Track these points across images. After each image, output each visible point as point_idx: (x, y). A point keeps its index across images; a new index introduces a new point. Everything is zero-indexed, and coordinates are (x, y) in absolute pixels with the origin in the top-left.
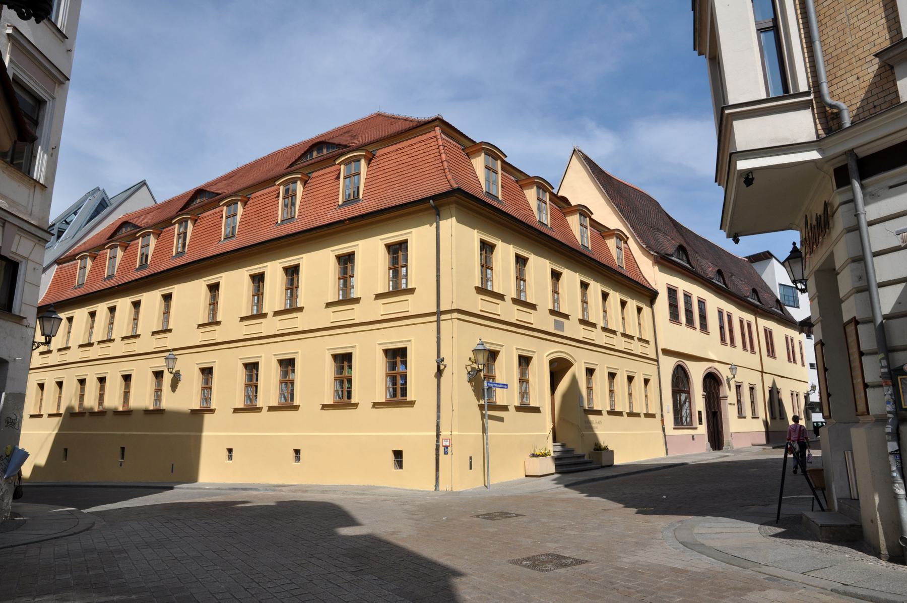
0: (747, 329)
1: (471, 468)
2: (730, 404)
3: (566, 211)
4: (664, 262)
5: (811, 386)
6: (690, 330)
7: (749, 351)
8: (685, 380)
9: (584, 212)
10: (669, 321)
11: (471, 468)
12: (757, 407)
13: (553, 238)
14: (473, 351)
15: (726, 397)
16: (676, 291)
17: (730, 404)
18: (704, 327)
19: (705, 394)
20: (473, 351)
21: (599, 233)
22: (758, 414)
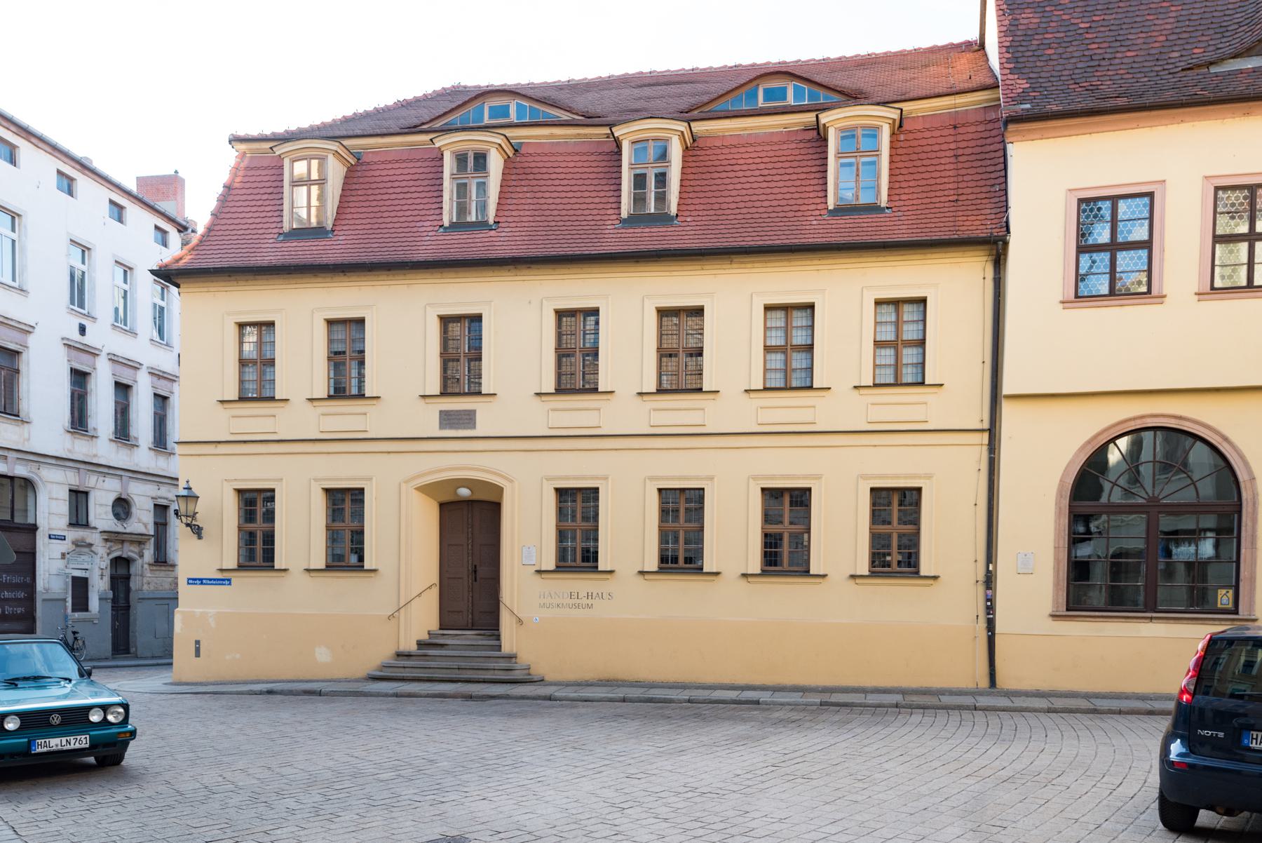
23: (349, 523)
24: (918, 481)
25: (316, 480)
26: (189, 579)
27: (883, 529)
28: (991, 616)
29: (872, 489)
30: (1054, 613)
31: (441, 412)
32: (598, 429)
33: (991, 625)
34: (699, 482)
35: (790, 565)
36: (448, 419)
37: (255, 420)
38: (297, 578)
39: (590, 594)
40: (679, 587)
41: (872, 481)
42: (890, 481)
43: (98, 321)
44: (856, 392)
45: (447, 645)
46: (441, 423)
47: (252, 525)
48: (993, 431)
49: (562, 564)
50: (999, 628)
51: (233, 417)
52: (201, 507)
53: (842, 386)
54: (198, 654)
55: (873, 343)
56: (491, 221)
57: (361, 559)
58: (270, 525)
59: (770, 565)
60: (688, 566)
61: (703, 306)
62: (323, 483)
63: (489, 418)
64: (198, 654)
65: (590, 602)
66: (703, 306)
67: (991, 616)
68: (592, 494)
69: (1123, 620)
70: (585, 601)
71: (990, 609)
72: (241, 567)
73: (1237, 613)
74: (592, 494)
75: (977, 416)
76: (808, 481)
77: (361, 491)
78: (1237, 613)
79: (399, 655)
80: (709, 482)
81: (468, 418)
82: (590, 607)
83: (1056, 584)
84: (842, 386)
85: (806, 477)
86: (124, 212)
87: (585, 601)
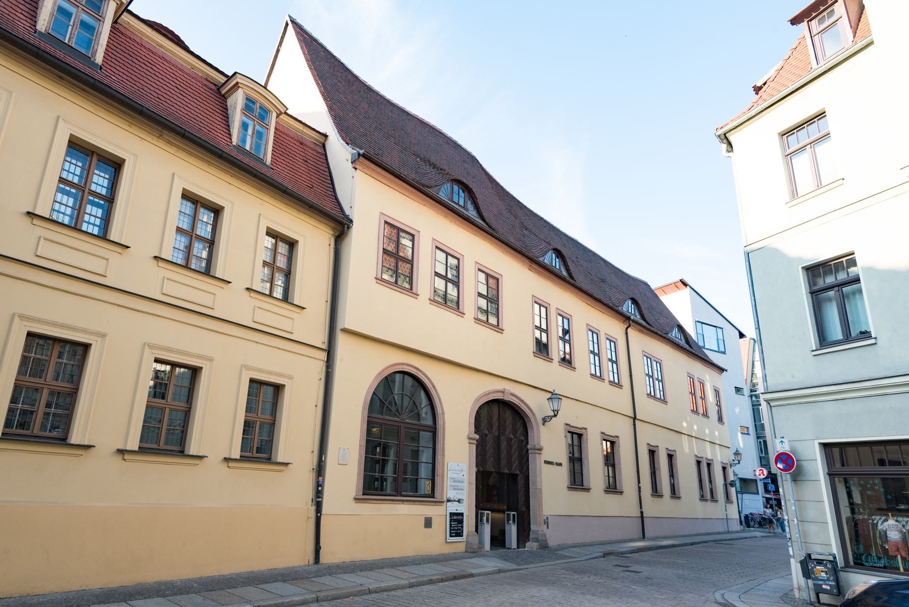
2: (547, 462)
17: (547, 462)
19: (477, 437)
24: (283, 379)
28: (320, 499)
29: (30, 334)
30: (357, 497)
33: (319, 506)
34: (87, 336)
35: (166, 443)
40: (257, 474)
41: (252, 372)
42: (264, 375)
43: (623, 387)
44: (247, 293)
47: (37, 380)
48: (330, 352)
49: (8, 430)
50: (325, 510)
55: (58, 178)
61: (124, 160)
66: (124, 160)
67: (320, 499)
69: (390, 502)
71: (318, 493)
74: (278, 389)
75: (320, 340)
76: (201, 361)
77: (86, 347)
78: (433, 497)
80: (99, 340)
83: (359, 474)
85: (199, 357)
86: (827, 471)
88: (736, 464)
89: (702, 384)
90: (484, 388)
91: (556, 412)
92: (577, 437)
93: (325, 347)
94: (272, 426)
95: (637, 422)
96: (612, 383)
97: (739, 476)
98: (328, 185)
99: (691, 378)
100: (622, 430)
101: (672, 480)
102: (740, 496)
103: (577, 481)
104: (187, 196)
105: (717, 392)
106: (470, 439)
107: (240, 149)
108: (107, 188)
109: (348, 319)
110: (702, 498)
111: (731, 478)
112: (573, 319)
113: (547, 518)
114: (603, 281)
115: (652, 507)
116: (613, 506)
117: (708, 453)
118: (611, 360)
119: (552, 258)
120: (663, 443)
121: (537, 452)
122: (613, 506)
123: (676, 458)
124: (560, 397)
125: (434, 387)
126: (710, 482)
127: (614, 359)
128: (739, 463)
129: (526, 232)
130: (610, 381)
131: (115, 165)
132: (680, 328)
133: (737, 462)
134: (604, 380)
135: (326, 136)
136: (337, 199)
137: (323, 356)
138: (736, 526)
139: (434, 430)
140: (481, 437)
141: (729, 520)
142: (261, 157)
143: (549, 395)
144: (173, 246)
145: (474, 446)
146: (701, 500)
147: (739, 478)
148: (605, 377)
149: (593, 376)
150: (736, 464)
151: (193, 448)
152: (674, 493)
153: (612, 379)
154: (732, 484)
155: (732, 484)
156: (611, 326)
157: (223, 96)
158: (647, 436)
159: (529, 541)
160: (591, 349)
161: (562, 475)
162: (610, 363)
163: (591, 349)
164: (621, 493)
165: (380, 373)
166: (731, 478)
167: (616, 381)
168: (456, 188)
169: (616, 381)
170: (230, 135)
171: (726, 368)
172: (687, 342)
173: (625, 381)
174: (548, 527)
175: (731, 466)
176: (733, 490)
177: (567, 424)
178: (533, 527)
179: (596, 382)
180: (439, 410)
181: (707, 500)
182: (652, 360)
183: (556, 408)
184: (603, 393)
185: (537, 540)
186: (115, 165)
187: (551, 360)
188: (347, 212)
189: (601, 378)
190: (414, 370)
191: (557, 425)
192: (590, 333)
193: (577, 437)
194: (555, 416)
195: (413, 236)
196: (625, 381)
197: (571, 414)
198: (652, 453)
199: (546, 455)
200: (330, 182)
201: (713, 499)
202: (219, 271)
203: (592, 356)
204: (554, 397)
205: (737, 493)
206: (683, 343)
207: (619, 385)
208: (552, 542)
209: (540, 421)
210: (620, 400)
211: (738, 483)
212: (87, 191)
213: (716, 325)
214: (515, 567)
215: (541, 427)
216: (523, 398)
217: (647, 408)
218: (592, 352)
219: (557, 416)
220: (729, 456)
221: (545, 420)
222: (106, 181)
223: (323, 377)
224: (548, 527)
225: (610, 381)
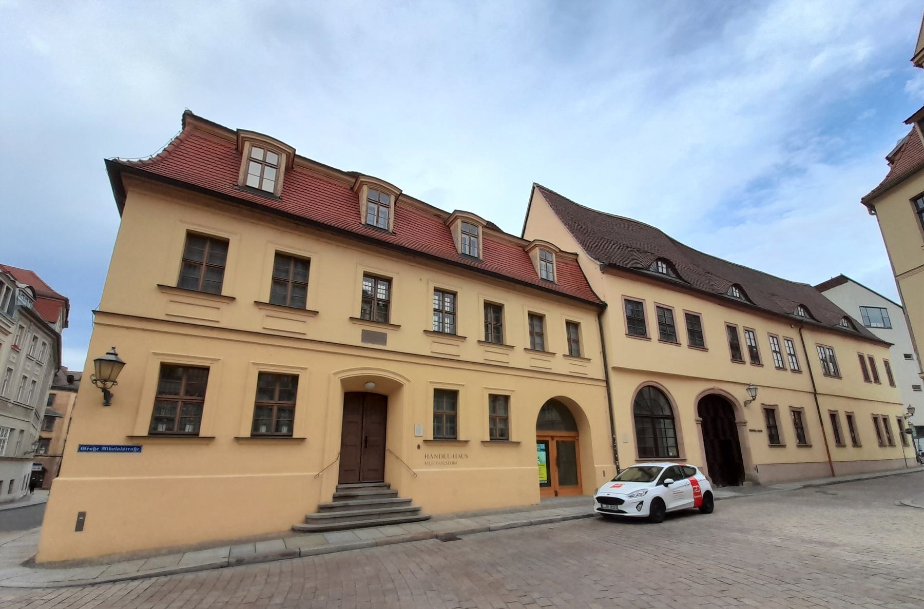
0: (665, 315)
1: (604, 472)
2: (751, 431)
3: (528, 249)
4: (610, 268)
5: (908, 409)
6: (669, 348)
7: (873, 383)
8: (662, 401)
9: (547, 247)
10: (625, 336)
11: (604, 472)
12: (808, 432)
13: (307, 219)
14: (94, 360)
15: (745, 423)
16: (735, 328)
17: (751, 431)
18: (877, 380)
19: (701, 419)
20: (94, 360)
21: (521, 249)
22: (685, 455)
23: (500, 413)
25: (254, 364)
26: (81, 446)
27: (265, 401)
31: (363, 330)
32: (458, 357)
36: (366, 336)
37: (445, 348)
38: (475, 448)
39: (427, 455)
43: (709, 351)
45: (357, 496)
46: (362, 339)
48: (607, 381)
49: (255, 433)
51: (532, 358)
52: (123, 376)
53: (245, 299)
54: (80, 526)
56: (391, 230)
57: (291, 429)
58: (453, 412)
59: (501, 437)
60: (502, 438)
61: (392, 278)
62: (261, 367)
63: (394, 341)
64: (80, 526)
65: (455, 460)
66: (392, 278)
68: (506, 398)
70: (452, 460)
72: (154, 434)
73: (679, 457)
74: (506, 398)
75: (601, 376)
78: (679, 457)
79: (322, 508)
81: (382, 338)
82: (455, 463)
84: (245, 299)
87: (452, 460)
88: (910, 416)
89: (871, 360)
90: (698, 390)
91: (754, 397)
92: (770, 413)
93: (604, 379)
94: (506, 420)
95: (818, 396)
96: (794, 371)
97: (915, 425)
98: (584, 282)
99: (861, 358)
100: (806, 403)
101: (853, 435)
102: (916, 440)
103: (775, 439)
104: (437, 290)
105: (886, 363)
106: (697, 421)
107: (259, 191)
108: (377, 293)
109: (613, 362)
110: (882, 445)
111: (907, 427)
112: (756, 331)
113: (757, 466)
114: (773, 295)
115: (838, 455)
116: (803, 455)
117: (881, 410)
118: (790, 354)
119: (733, 291)
120: (842, 408)
121: (743, 424)
122: (803, 455)
123: (839, 417)
124: (757, 387)
125: (669, 392)
126: (888, 432)
127: (792, 353)
128: (913, 415)
129: (709, 275)
130: (792, 370)
131: (389, 281)
132: (847, 318)
133: (911, 415)
134: (786, 369)
135: (577, 255)
136: (593, 291)
137: (605, 384)
138: (913, 462)
139: (672, 418)
140: (703, 419)
141: (668, 439)
142: (476, 256)
143: (747, 387)
144: (432, 323)
145: (700, 425)
146: (880, 446)
147: (914, 426)
148: (787, 366)
149: (778, 368)
150: (910, 416)
151: (462, 436)
152: (856, 443)
153: (792, 368)
154: (909, 431)
155: (909, 431)
156: (783, 331)
157: (526, 252)
158: (827, 405)
159: (745, 481)
160: (773, 349)
161: (764, 438)
162: (790, 357)
163: (773, 349)
164: (811, 446)
165: (637, 389)
166: (907, 427)
167: (796, 368)
168: (660, 263)
169: (796, 368)
170: (536, 273)
171: (893, 343)
172: (854, 328)
173: (804, 367)
174: (758, 472)
175: (905, 418)
176: (909, 437)
177: (762, 404)
178: (746, 472)
179: (797, 375)
180: (674, 405)
181: (885, 446)
182: (825, 348)
183: (754, 395)
184: (787, 379)
185: (750, 480)
186: (389, 281)
187: (744, 363)
188: (602, 299)
189: (783, 369)
190: (655, 383)
191: (756, 406)
192: (771, 338)
193: (770, 413)
194: (754, 399)
195: (671, 310)
196: (804, 367)
197: (766, 398)
198: (833, 416)
199: (750, 426)
200: (586, 282)
201: (891, 443)
202: (460, 332)
203: (775, 354)
204: (750, 387)
205: (913, 438)
206: (851, 329)
207: (799, 371)
208: (761, 480)
209: (742, 404)
210: (802, 381)
211: (914, 430)
212: (444, 312)
213: (880, 307)
214: (743, 495)
215: (745, 410)
216: (728, 391)
217: (824, 384)
218: (775, 351)
219: (756, 400)
220: (902, 411)
221: (746, 403)
222: (384, 291)
223: (607, 396)
224: (758, 472)
225: (792, 370)
